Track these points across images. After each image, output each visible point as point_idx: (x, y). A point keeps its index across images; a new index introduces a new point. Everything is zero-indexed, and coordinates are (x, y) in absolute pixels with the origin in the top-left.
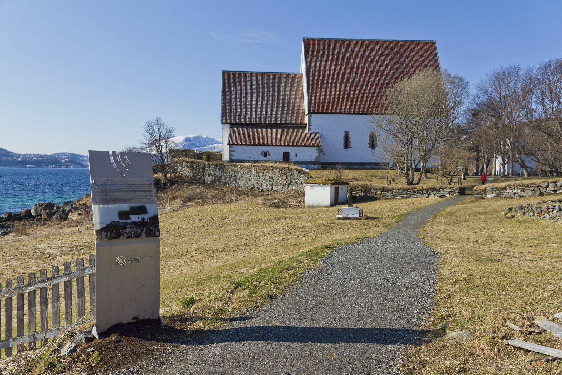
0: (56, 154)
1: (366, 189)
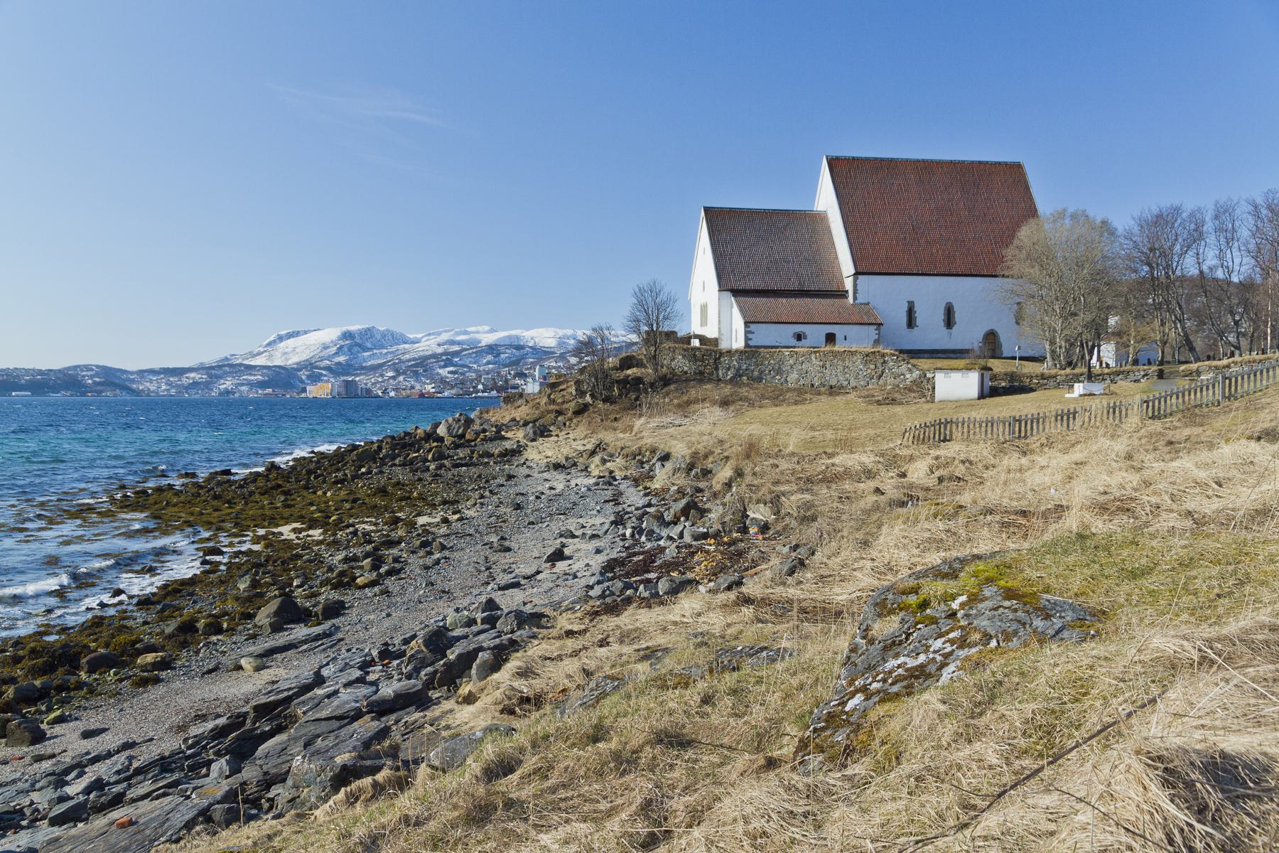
0: (69, 368)
1: (1012, 376)
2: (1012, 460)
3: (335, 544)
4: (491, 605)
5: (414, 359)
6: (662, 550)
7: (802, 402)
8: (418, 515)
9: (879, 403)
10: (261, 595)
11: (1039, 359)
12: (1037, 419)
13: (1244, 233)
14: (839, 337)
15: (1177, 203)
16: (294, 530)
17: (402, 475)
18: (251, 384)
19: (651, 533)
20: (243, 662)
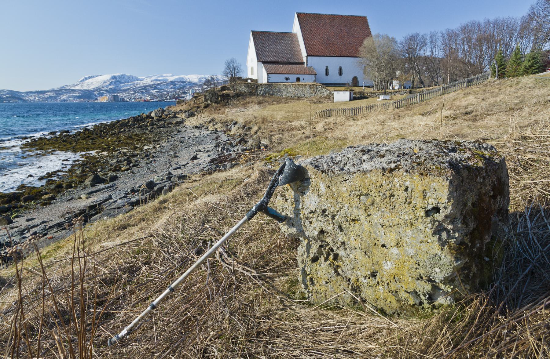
1: (361, 93)
2: (352, 122)
3: (113, 157)
4: (170, 173)
5: (142, 87)
6: (231, 155)
7: (288, 103)
8: (144, 146)
9: (315, 103)
10: (86, 175)
11: (372, 87)
12: (361, 109)
13: (439, 43)
14: (301, 79)
15: (418, 32)
16: (97, 152)
17: (138, 131)
18: (74, 97)
19: (227, 149)
20: (82, 196)
